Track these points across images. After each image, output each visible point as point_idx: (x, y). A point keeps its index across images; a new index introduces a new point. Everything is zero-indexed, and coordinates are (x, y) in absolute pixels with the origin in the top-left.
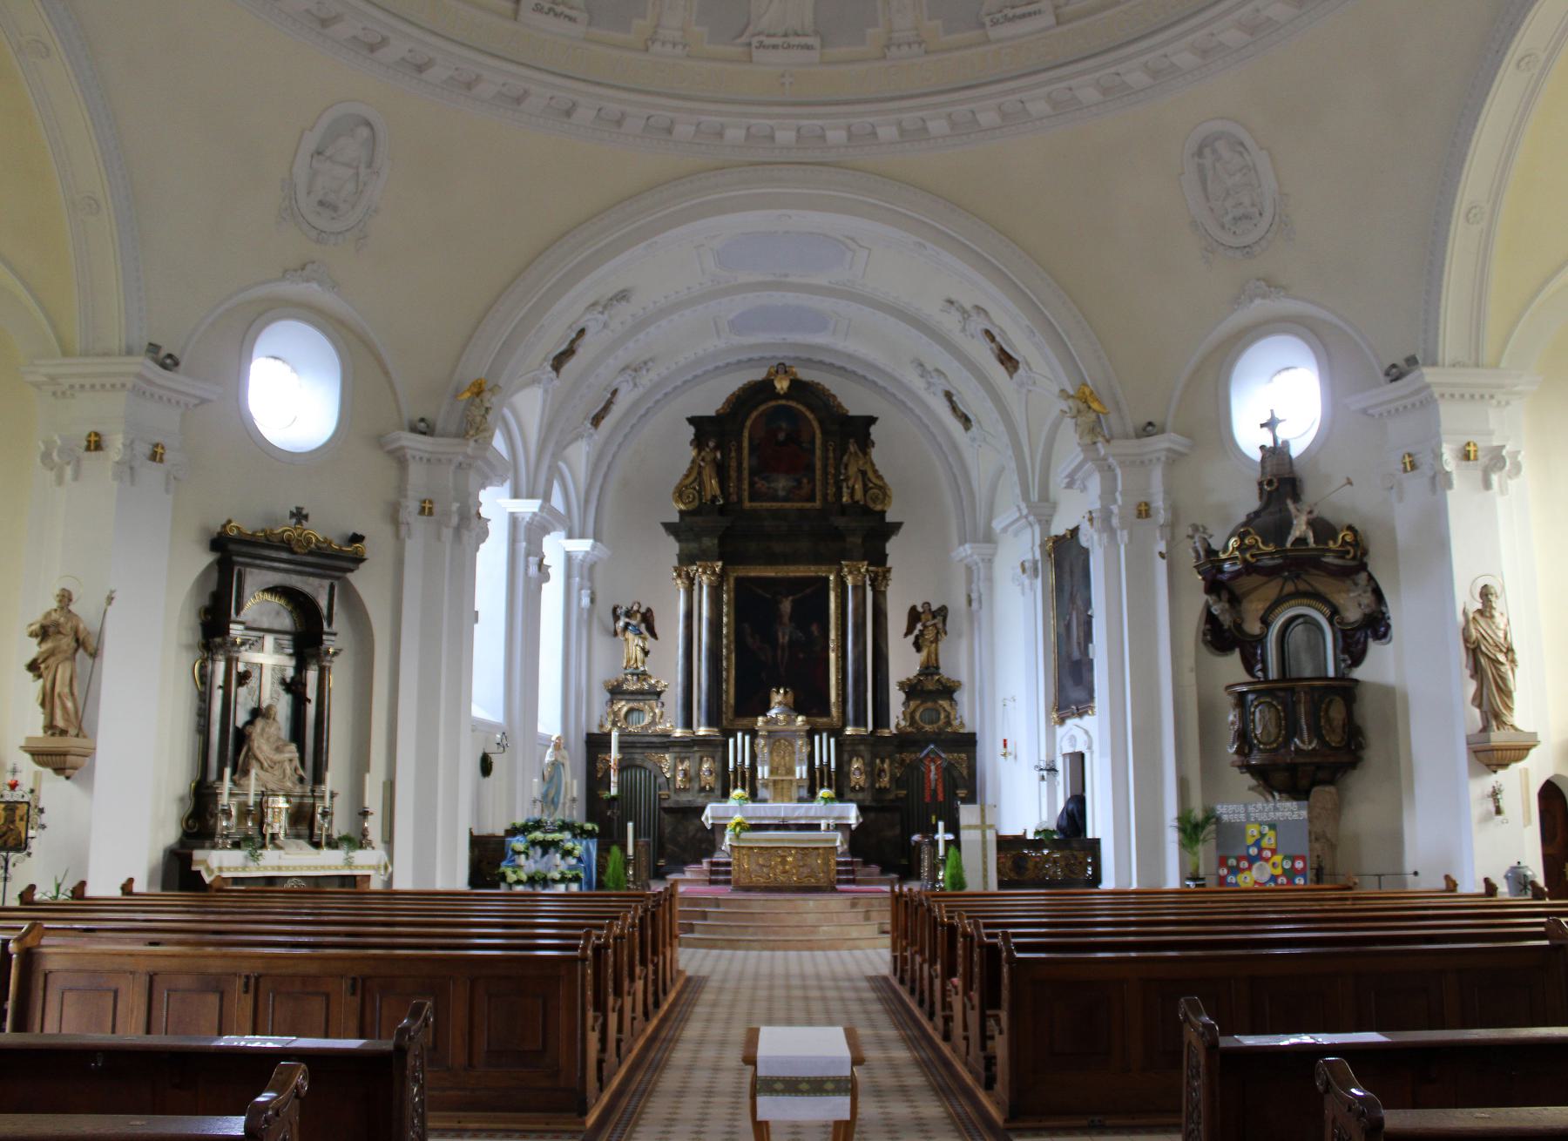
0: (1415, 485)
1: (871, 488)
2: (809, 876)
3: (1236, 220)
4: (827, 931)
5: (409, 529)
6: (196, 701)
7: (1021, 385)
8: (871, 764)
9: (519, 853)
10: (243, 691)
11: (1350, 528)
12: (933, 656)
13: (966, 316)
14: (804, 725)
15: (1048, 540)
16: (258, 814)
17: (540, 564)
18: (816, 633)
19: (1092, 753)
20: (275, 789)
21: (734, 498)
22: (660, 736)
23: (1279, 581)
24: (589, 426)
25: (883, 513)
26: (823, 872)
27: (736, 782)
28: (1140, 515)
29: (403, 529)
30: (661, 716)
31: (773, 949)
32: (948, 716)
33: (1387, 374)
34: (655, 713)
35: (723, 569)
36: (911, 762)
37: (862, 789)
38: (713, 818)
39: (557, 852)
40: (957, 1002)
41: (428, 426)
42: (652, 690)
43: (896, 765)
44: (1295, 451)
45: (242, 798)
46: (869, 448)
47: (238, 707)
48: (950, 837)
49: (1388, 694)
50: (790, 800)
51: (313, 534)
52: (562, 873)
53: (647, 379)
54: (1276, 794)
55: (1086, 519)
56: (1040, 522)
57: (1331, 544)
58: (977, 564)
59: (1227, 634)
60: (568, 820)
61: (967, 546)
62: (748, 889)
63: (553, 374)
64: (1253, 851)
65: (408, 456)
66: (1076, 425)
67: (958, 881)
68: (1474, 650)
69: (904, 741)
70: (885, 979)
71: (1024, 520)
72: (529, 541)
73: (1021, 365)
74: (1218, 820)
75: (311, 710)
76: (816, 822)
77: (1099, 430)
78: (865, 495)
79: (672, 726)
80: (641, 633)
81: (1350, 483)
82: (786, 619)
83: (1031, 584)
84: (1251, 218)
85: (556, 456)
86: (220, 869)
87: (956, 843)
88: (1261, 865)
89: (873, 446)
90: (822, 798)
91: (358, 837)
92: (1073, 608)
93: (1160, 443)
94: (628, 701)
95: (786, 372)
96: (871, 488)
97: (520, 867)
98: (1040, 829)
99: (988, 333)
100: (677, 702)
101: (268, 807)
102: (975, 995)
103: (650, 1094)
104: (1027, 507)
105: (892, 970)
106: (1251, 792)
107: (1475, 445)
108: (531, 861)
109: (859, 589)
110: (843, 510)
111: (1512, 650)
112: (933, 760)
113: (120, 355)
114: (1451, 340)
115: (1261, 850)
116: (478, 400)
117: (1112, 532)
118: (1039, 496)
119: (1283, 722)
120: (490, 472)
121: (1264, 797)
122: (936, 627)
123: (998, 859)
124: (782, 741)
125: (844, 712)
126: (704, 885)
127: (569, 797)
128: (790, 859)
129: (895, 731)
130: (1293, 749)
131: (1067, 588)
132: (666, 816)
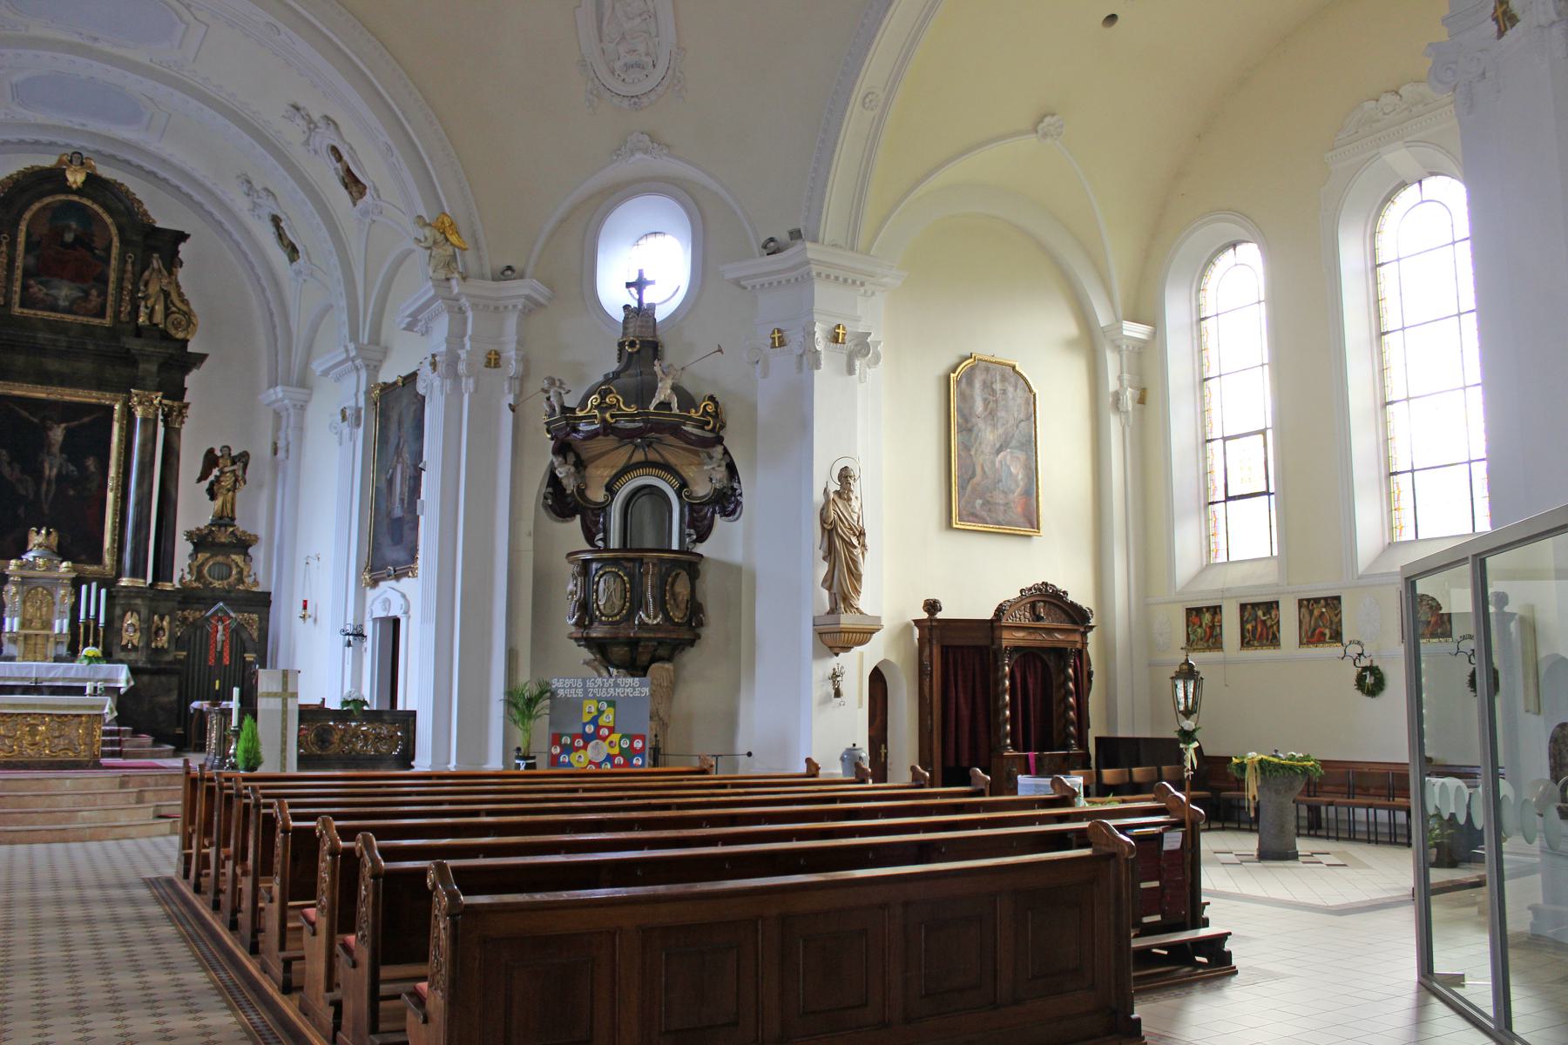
0: (781, 360)
1: (173, 312)
3: (628, 67)
4: (88, 817)
7: (365, 213)
8: (149, 620)
11: (712, 398)
12: (229, 506)
13: (312, 126)
14: (68, 571)
18: (92, 468)
19: (409, 618)
23: (630, 448)
25: (185, 342)
26: (85, 744)
28: (488, 365)
31: (12, 843)
32: (241, 572)
36: (194, 620)
37: (135, 648)
43: (178, 623)
44: (661, 314)
46: (176, 267)
49: (733, 572)
50: (45, 659)
54: (614, 671)
55: (427, 363)
56: (367, 366)
57: (693, 413)
58: (287, 410)
59: (569, 499)
61: (279, 389)
64: (590, 729)
66: (431, 255)
67: (253, 761)
68: (830, 531)
69: (186, 597)
70: (170, 882)
71: (350, 363)
73: (368, 191)
74: (553, 694)
77: (454, 264)
81: (720, 350)
82: (56, 449)
84: (643, 68)
88: (597, 743)
89: (181, 266)
90: (86, 656)
92: (398, 462)
93: (517, 289)
95: (82, 164)
96: (173, 312)
98: (350, 699)
99: (334, 150)
104: (356, 348)
106: (586, 666)
107: (844, 328)
109: (151, 423)
110: (139, 332)
111: (864, 534)
112: (220, 620)
114: (832, 222)
115: (598, 728)
117: (455, 376)
119: (628, 594)
121: (598, 671)
123: (300, 730)
124: (40, 589)
125: (119, 560)
129: (178, 586)
130: (636, 622)
131: (393, 440)
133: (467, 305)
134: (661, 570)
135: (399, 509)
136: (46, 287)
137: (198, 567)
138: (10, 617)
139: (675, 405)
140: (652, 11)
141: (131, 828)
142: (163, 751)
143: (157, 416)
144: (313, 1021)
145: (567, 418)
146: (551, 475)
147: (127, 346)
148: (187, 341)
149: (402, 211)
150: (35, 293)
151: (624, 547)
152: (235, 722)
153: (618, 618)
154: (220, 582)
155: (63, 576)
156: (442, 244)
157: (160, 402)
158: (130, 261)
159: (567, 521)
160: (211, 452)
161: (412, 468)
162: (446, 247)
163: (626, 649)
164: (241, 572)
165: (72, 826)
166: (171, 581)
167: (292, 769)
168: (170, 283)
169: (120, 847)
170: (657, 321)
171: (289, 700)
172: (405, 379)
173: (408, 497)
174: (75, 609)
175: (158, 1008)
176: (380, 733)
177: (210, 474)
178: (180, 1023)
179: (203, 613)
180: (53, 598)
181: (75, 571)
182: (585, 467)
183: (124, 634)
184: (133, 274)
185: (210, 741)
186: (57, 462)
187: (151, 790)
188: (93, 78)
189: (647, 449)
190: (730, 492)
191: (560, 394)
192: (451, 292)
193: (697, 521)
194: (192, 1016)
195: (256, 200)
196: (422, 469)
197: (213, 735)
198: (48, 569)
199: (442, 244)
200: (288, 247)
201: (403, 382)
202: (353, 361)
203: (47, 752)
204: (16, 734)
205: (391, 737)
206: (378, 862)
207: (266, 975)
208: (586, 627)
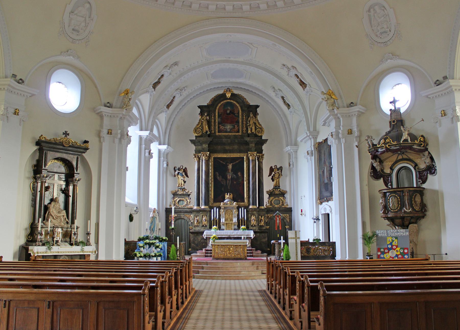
0: (445, 121)
1: (257, 128)
2: (238, 255)
3: (381, 33)
4: (244, 273)
5: (104, 139)
6: (31, 196)
7: (307, 92)
8: (258, 217)
9: (141, 247)
10: (47, 193)
11: (422, 136)
16: (52, 234)
17: (150, 153)
18: (240, 175)
20: (58, 226)
21: (213, 132)
22: (189, 209)
23: (397, 155)
24: (166, 108)
25: (262, 136)
26: (243, 253)
27: (214, 223)
28: (348, 134)
29: (102, 139)
31: (226, 279)
32: (283, 202)
33: (435, 83)
34: (188, 201)
35: (209, 154)
37: (255, 226)
38: (206, 235)
40: (296, 307)
41: (110, 105)
42: (187, 194)
44: (402, 111)
45: (46, 229)
46: (257, 115)
47: (45, 198)
48: (284, 241)
49: (435, 192)
50: (232, 230)
51: (71, 140)
52: (155, 254)
53: (185, 93)
54: (397, 227)
55: (330, 135)
56: (313, 137)
60: (157, 236)
61: (289, 147)
62: (217, 259)
63: (153, 90)
64: (390, 246)
65: (104, 115)
67: (288, 257)
69: (268, 210)
70: (265, 291)
72: (145, 145)
74: (377, 236)
75: (71, 199)
76: (241, 236)
78: (255, 131)
79: (193, 205)
81: (423, 120)
82: (230, 171)
85: (155, 117)
86: (38, 253)
87: (286, 243)
90: (242, 228)
91: (85, 242)
93: (355, 109)
94: (179, 197)
95: (230, 91)
96: (257, 128)
97: (141, 251)
99: (296, 75)
100: (195, 198)
101: (55, 232)
102: (305, 305)
103: (193, 309)
106: (388, 226)
108: (145, 250)
109: (254, 161)
110: (249, 135)
113: (3, 78)
115: (392, 246)
116: (127, 96)
117: (339, 139)
120: (132, 121)
121: (392, 228)
124: (229, 210)
125: (249, 201)
126: (203, 257)
127: (158, 228)
128: (231, 249)
129: (265, 207)
130: (403, 211)
132: (191, 235)
134: (410, 194)
136: (224, 126)
137: (271, 201)
139: (409, 140)
140: (387, 14)
141: (255, 277)
142: (264, 255)
143: (256, 159)
144: (296, 327)
145: (374, 148)
146: (372, 167)
147: (246, 140)
151: (398, 187)
152: (282, 246)
153: (397, 210)
155: (235, 206)
156: (330, 99)
157: (256, 154)
159: (378, 180)
160: (271, 167)
162: (331, 100)
163: (400, 220)
165: (240, 276)
166: (263, 206)
167: (299, 259)
168: (256, 120)
169: (252, 282)
170: (402, 113)
174: (238, 215)
175: (259, 321)
176: (325, 249)
178: (264, 325)
179: (273, 215)
181: (237, 205)
182: (383, 163)
184: (246, 119)
185: (276, 252)
186: (231, 174)
187: (260, 266)
188: (230, 68)
189: (402, 155)
190: (432, 166)
191: (372, 140)
192: (335, 113)
193: (422, 177)
194: (267, 324)
195: (277, 93)
196: (332, 168)
198: (231, 204)
205: (329, 250)
206: (309, 283)
207: (287, 316)
208: (386, 214)
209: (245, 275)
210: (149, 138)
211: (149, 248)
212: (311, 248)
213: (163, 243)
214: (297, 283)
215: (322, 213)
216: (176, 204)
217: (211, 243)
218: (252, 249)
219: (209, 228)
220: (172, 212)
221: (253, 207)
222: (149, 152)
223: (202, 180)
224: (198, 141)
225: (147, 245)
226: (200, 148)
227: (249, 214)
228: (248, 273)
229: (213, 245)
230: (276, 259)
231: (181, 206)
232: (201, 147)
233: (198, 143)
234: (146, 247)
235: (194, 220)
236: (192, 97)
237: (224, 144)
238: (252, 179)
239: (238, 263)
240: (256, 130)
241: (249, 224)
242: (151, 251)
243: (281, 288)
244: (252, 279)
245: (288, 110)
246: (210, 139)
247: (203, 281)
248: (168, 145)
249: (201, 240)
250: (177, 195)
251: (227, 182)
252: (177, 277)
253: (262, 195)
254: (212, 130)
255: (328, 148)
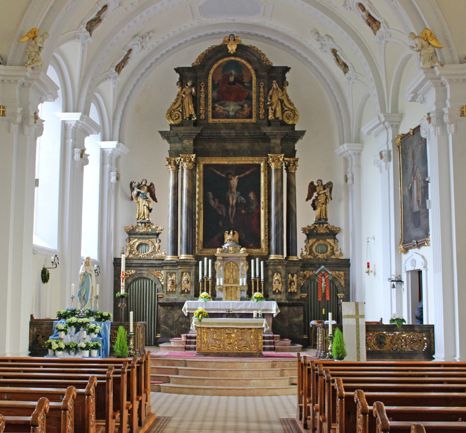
1: (286, 111)
2: (246, 347)
4: (256, 383)
7: (382, 38)
8: (286, 277)
9: (61, 330)
12: (324, 212)
14: (244, 253)
15: (398, 137)
18: (252, 198)
19: (427, 270)
21: (203, 116)
22: (158, 260)
24: (114, 71)
25: (293, 125)
26: (254, 344)
27: (203, 287)
30: (159, 248)
31: (220, 395)
32: (333, 249)
34: (155, 246)
35: (196, 159)
36: (310, 276)
37: (280, 293)
38: (188, 309)
39: (85, 330)
42: (153, 232)
43: (301, 278)
48: (334, 322)
50: (236, 299)
52: (87, 344)
53: (150, 44)
55: (426, 118)
56: (392, 126)
58: (351, 156)
60: (92, 310)
61: (345, 145)
62: (206, 354)
63: (88, 34)
66: (420, 55)
67: (341, 355)
70: (293, 421)
71: (382, 125)
72: (74, 139)
73: (381, 25)
76: (251, 312)
77: (435, 58)
79: (165, 254)
80: (147, 198)
82: (234, 190)
83: (386, 165)
87: (339, 326)
89: (288, 85)
90: (255, 297)
95: (234, 40)
96: (286, 111)
97: (61, 339)
98: (394, 318)
100: (168, 240)
104: (385, 116)
105: (299, 417)
108: (68, 336)
109: (279, 171)
110: (269, 123)
116: (34, 42)
118: (392, 111)
122: (325, 195)
124: (232, 263)
125: (269, 246)
127: (94, 295)
128: (233, 335)
129: (300, 258)
133: (446, 81)
135: (417, 207)
136: (222, 106)
138: (219, 278)
142: (296, 348)
143: (282, 167)
147: (264, 131)
148: (295, 125)
149: (402, 32)
150: (218, 111)
154: (322, 255)
155: (242, 255)
156: (426, 46)
157: (283, 159)
158: (262, 86)
160: (312, 183)
161: (422, 181)
162: (429, 49)
164: (333, 249)
166: (296, 255)
167: (364, 360)
168: (283, 95)
169: (271, 400)
171: (360, 319)
172: (414, 130)
173: (422, 199)
177: (313, 195)
180: (238, 268)
181: (247, 252)
183: (274, 285)
184: (264, 93)
185: (318, 343)
186: (235, 196)
195: (323, 43)
196: (428, 182)
197: (320, 339)
198: (235, 252)
199: (426, 46)
200: (342, 65)
201: (413, 132)
202: (384, 124)
203: (236, 348)
204: (221, 339)
205: (420, 340)
209: (258, 387)
210: (80, 127)
211: (76, 332)
212: (386, 336)
213: (103, 324)
214: (359, 417)
215: (407, 270)
216: (133, 251)
217: (194, 325)
218: (273, 336)
219: (193, 296)
220: (121, 266)
221: (276, 257)
222: (81, 152)
223: (182, 206)
224: (175, 134)
225: (73, 327)
226: (179, 147)
227: (268, 269)
228: (263, 382)
229: (199, 327)
230: (318, 355)
231: (143, 254)
232: (181, 145)
233: (174, 138)
234: (70, 330)
235: (167, 281)
236: (164, 51)
237: (224, 140)
238: (276, 204)
239: (245, 362)
240: (283, 113)
241: (269, 289)
242: (81, 338)
243: (324, 420)
244: (270, 396)
245: (345, 75)
246: (197, 130)
247: (176, 398)
248: (119, 141)
249: (178, 319)
250: (136, 234)
251: (228, 210)
252: (107, 395)
253: (294, 233)
254: (201, 114)
255: (420, 144)
